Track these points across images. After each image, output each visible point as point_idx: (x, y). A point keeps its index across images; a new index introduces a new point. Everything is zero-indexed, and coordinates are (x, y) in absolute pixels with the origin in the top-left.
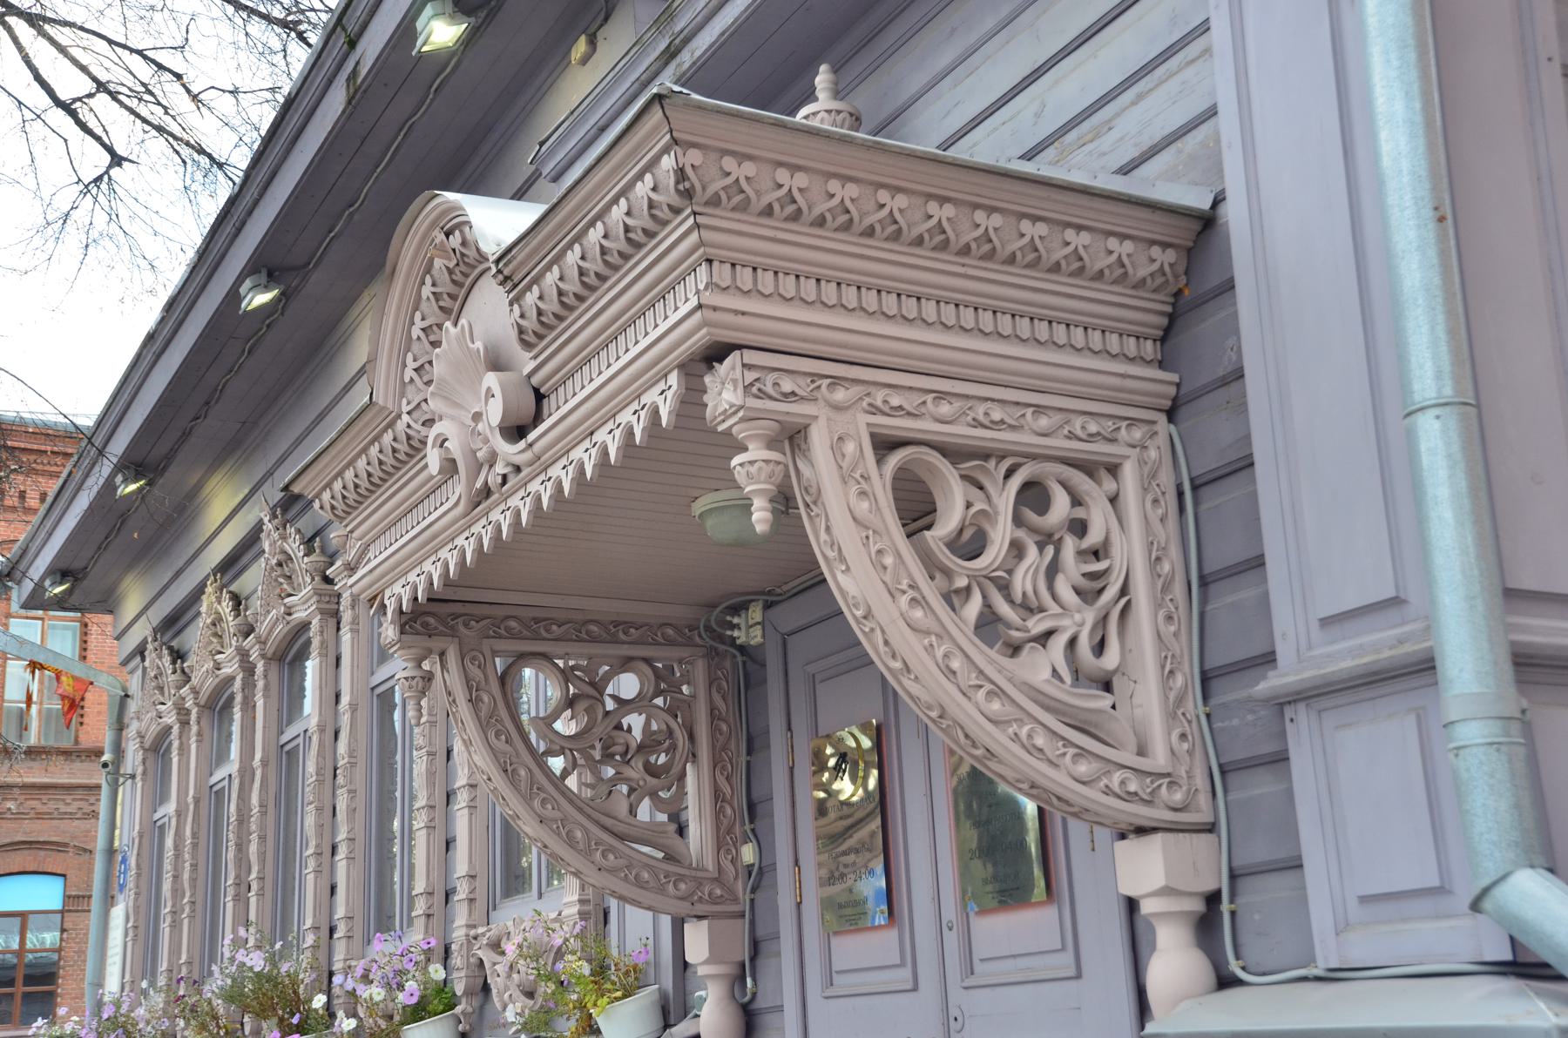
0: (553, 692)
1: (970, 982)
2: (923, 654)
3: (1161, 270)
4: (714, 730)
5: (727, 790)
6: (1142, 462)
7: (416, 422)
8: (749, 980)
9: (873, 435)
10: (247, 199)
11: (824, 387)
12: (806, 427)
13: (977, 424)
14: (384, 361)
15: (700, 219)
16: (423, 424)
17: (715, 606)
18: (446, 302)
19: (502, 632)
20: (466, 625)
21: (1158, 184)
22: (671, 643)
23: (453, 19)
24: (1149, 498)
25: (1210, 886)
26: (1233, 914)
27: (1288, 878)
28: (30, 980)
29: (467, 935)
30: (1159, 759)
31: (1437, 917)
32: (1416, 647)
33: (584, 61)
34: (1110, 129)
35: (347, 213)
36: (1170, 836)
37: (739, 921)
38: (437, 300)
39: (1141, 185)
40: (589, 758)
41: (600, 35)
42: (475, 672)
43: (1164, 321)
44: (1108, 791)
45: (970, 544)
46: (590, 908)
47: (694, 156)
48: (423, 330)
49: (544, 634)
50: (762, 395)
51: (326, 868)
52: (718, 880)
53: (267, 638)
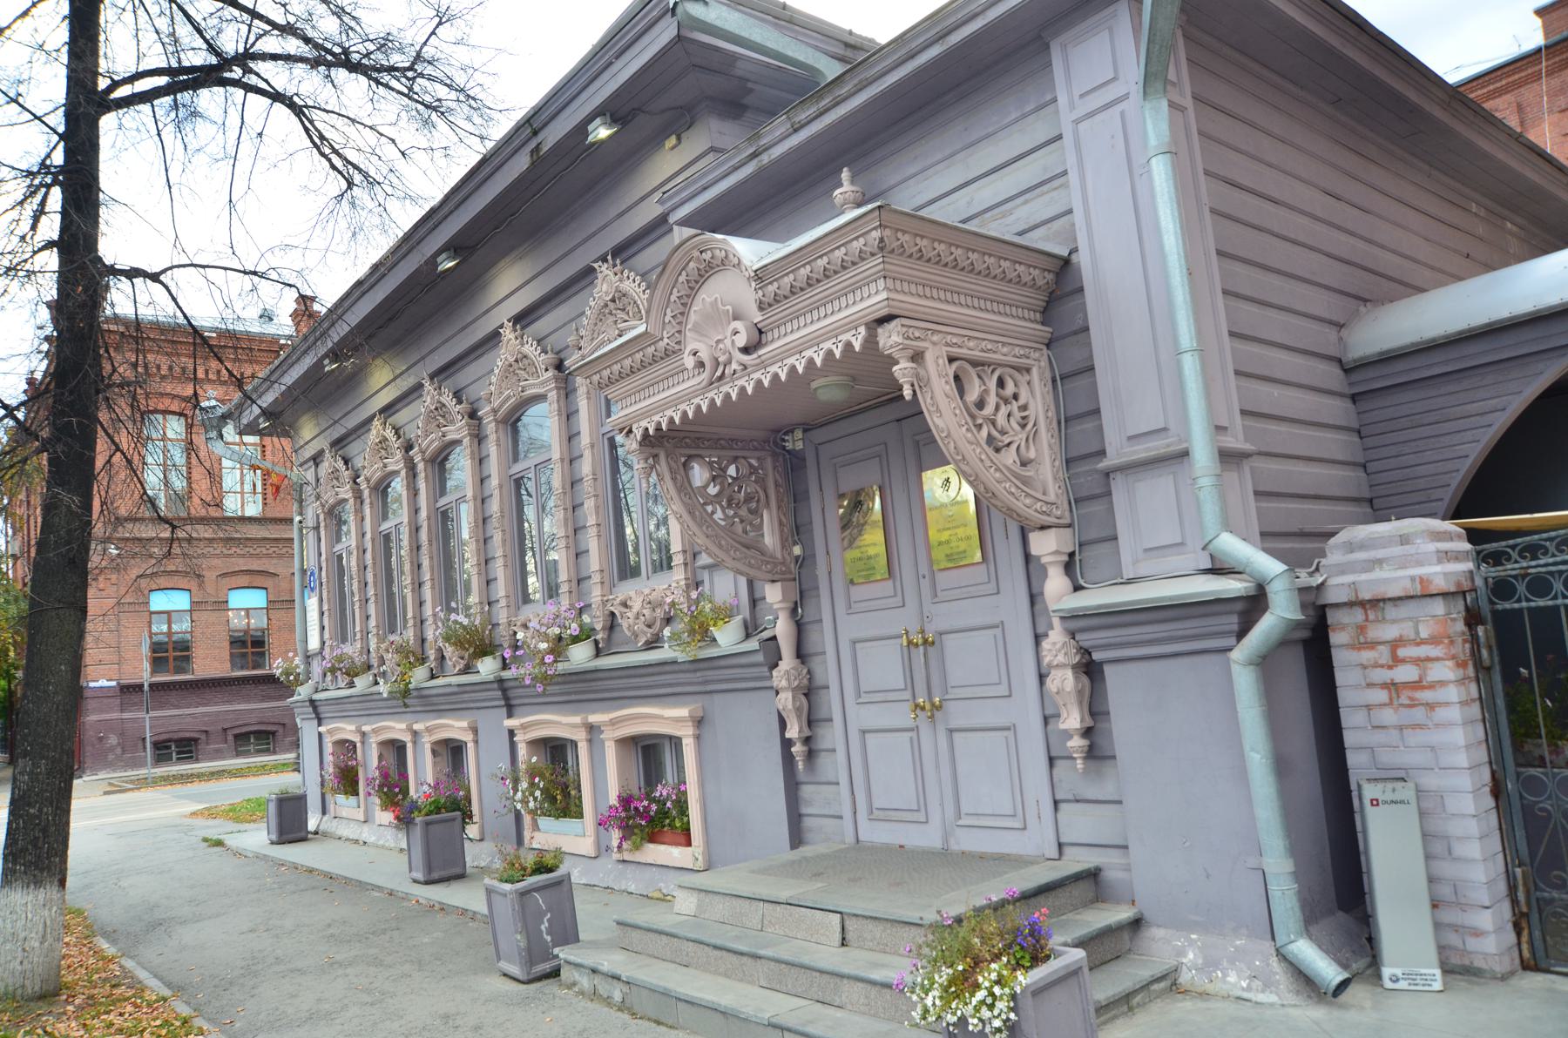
0: (706, 475)
1: (936, 600)
3: (1048, 283)
4: (777, 492)
5: (784, 520)
6: (1040, 367)
8: (800, 610)
10: (446, 210)
12: (923, 352)
13: (983, 351)
17: (779, 431)
21: (1036, 240)
22: (756, 449)
23: (610, 126)
25: (1071, 550)
26: (1080, 561)
27: (1113, 542)
28: (166, 659)
30: (1052, 497)
33: (673, 148)
39: (1030, 240)
40: (722, 507)
41: (683, 135)
42: (673, 464)
44: (1036, 511)
45: (981, 404)
46: (690, 582)
47: (887, 232)
50: (908, 338)
51: (483, 571)
52: (783, 563)
53: (426, 450)
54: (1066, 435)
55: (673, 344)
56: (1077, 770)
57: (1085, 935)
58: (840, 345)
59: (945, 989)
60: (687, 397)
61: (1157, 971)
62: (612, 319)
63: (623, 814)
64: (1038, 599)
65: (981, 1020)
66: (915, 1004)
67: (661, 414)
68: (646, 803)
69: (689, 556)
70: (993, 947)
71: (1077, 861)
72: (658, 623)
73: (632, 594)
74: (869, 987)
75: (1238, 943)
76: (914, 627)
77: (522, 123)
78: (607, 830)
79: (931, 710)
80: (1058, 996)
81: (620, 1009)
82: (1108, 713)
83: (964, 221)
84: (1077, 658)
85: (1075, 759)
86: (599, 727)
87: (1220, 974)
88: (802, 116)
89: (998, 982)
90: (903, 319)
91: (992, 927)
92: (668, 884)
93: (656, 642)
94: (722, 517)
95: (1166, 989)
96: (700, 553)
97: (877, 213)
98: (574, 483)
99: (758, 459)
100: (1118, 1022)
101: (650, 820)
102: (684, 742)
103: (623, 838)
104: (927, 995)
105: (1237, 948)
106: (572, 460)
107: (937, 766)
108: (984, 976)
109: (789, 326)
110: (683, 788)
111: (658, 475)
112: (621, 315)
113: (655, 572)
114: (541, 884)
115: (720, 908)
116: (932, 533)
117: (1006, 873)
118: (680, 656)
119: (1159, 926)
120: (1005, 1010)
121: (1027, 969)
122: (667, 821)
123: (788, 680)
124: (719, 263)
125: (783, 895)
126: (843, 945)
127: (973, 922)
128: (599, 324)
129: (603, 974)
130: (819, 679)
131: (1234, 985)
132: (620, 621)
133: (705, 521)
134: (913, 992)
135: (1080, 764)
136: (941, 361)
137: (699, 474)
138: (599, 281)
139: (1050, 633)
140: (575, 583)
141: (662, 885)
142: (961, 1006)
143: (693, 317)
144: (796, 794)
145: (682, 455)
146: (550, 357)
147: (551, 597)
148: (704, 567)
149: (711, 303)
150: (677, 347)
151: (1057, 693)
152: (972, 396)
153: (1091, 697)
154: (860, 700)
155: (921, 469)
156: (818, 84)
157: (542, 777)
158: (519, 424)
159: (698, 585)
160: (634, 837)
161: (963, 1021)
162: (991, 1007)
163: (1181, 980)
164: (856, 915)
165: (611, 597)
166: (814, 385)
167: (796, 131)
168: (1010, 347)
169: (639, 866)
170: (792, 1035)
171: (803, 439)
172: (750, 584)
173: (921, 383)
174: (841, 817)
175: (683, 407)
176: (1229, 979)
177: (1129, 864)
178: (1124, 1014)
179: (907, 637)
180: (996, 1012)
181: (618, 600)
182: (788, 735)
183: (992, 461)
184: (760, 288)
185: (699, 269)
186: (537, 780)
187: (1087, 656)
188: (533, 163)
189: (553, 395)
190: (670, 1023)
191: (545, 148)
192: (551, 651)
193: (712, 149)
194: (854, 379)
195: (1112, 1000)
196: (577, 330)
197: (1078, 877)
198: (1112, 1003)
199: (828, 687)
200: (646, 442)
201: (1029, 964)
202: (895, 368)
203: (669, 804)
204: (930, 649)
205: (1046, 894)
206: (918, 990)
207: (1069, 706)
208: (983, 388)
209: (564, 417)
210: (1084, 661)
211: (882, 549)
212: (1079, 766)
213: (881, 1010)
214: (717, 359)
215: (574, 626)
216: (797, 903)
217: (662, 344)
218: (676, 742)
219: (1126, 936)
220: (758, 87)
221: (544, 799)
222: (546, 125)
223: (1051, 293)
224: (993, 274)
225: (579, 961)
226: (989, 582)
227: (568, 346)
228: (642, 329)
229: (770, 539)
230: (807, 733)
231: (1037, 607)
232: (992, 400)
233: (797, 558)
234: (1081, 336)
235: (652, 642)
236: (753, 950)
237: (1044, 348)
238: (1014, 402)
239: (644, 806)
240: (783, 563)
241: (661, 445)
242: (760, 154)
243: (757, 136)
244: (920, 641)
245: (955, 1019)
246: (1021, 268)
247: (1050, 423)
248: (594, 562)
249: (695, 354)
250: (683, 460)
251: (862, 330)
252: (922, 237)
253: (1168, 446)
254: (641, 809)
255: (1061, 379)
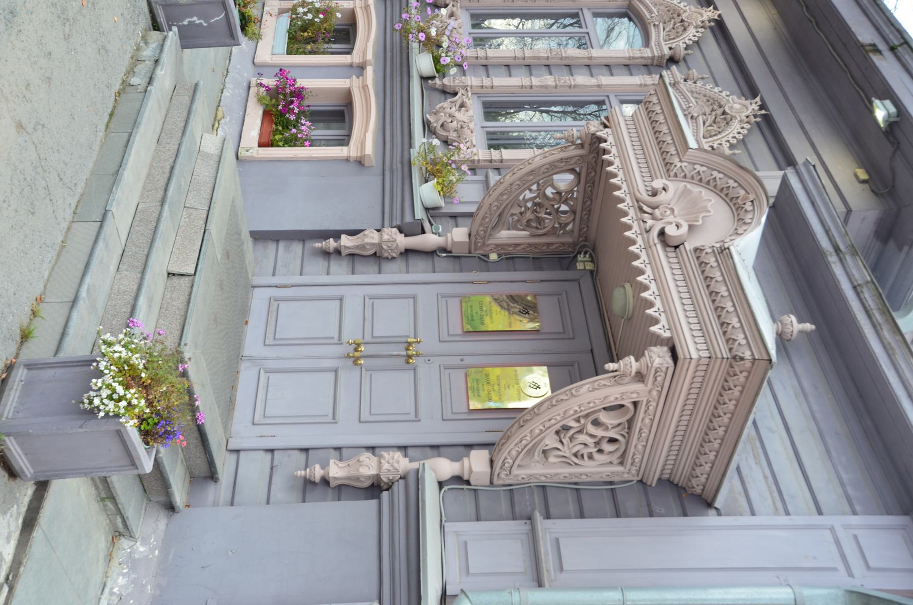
2: (557, 413)
3: (693, 487)
4: (544, 245)
6: (623, 473)
7: (677, 170)
8: (444, 255)
9: (639, 401)
11: (658, 388)
12: (643, 382)
14: (704, 156)
15: (725, 360)
16: (675, 173)
18: (725, 191)
19: (586, 199)
20: (594, 157)
21: (731, 483)
22: (580, 230)
23: (885, 121)
24: (610, 474)
25: (472, 482)
26: (463, 489)
27: (474, 517)
29: (468, 86)
30: (515, 471)
31: (460, 569)
32: (545, 576)
33: (856, 176)
34: (756, 463)
35: (813, 20)
36: (489, 473)
37: (467, 252)
38: (727, 187)
39: (732, 476)
40: (535, 198)
42: (574, 160)
43: (676, 482)
44: (506, 458)
45: (596, 423)
46: (476, 164)
47: (748, 364)
48: (715, 178)
49: (588, 185)
50: (656, 372)
52: (484, 244)
54: (566, 488)
55: (674, 171)
56: (297, 470)
57: (164, 467)
58: (657, 314)
59: (126, 362)
60: (628, 179)
61: (131, 522)
62: (708, 110)
63: (288, 91)
64: (435, 451)
65: (100, 389)
66: (116, 336)
67: (616, 155)
68: (296, 110)
69: (497, 164)
70: (158, 401)
71: (224, 464)
72: (444, 134)
73: (471, 113)
74: (133, 295)
75: (149, 587)
76: (421, 349)
77: (906, 36)
78: (276, 75)
79: (354, 357)
80: (115, 449)
81: (123, 82)
82: (339, 500)
83: (754, 423)
84: (385, 480)
85: (305, 469)
86: (362, 75)
87: (125, 571)
88: (867, 295)
89: (129, 404)
90: (673, 368)
91: (175, 401)
92: (227, 128)
93: (429, 130)
94: (526, 197)
95: (117, 528)
96: (500, 174)
97: (766, 357)
98: (569, 67)
99: (572, 231)
100: (93, 489)
101: (282, 113)
102: (345, 148)
103: (268, 89)
104: (123, 346)
105: (145, 586)
106: (590, 67)
107: (308, 357)
108: (135, 393)
109: (679, 272)
110: (307, 143)
111: (566, 147)
112: (710, 119)
113: (488, 133)
114: (232, 21)
115: (204, 173)
116: (498, 371)
117: (219, 407)
118: (414, 152)
119: (167, 525)
120: (107, 409)
121: (139, 427)
122: (280, 128)
123: (389, 241)
124: (741, 217)
125: (212, 227)
126: (169, 274)
127: (179, 386)
128: (705, 99)
129: (154, 69)
130: (386, 266)
131: (115, 582)
132: (449, 100)
133: (524, 184)
134: (125, 334)
135: (301, 473)
136: (634, 395)
137: (564, 180)
138: (743, 101)
139: (407, 460)
140: (484, 62)
141: (228, 119)
142: (112, 373)
143: (696, 189)
144: (295, 239)
145: (581, 168)
146: (682, 52)
147: (475, 39)
148: (487, 176)
149: (705, 207)
150: (672, 174)
151: (359, 461)
152: (603, 417)
153: (353, 487)
154: (367, 299)
155: (549, 366)
156: (894, 311)
157: (323, 21)
158: (626, 19)
159: (473, 170)
160: (268, 98)
161: (100, 374)
162: (110, 398)
163: (123, 540)
164: (192, 286)
165: (470, 94)
166: (627, 286)
167: (855, 288)
168: (642, 451)
169: (244, 100)
170: (97, 229)
171: (585, 269)
172: (470, 215)
173: (618, 378)
174: (274, 275)
175: (621, 174)
176: (121, 578)
177: (218, 505)
178: (99, 494)
179: (415, 342)
180: (106, 401)
181: (466, 100)
182: (343, 236)
183: (549, 428)
184: (713, 251)
185: (737, 198)
186: (321, 16)
187: (385, 487)
188: (862, 46)
189: (647, 53)
190: (111, 125)
191: (875, 58)
192: (428, 38)
193: (849, 211)
194: (629, 319)
195: (111, 486)
196: (702, 78)
197: (211, 464)
198: (108, 486)
199: (380, 273)
200: (595, 140)
201: (142, 428)
202: (632, 358)
203: (294, 130)
204: (403, 360)
205: (199, 439)
206: (127, 339)
207: (347, 469)
208: (610, 427)
209: (627, 62)
210: (382, 485)
211: (491, 327)
212: (299, 472)
213: (114, 303)
214: (657, 207)
215: (448, 60)
216: (205, 238)
217: (676, 160)
218: (344, 141)
219: (162, 498)
220: (903, 254)
221: (304, 21)
222: (899, 59)
223: (684, 489)
224: (704, 445)
225: (166, 49)
226: (453, 413)
227: (689, 69)
228: (692, 144)
229: (505, 235)
230: (344, 252)
231: (428, 450)
232: (599, 433)
233: (487, 256)
234: (646, 510)
235: (429, 127)
236: (168, 200)
237: (639, 478)
238: (596, 449)
239: (294, 109)
240: (484, 244)
241: (590, 152)
242: (838, 255)
243: (854, 253)
244: (410, 353)
245: (102, 368)
246: (707, 467)
247: (576, 477)
248: (501, 81)
249: (664, 189)
250: (578, 169)
251: (667, 334)
252: (741, 392)
253: (548, 571)
254: (291, 107)
255: (612, 489)
